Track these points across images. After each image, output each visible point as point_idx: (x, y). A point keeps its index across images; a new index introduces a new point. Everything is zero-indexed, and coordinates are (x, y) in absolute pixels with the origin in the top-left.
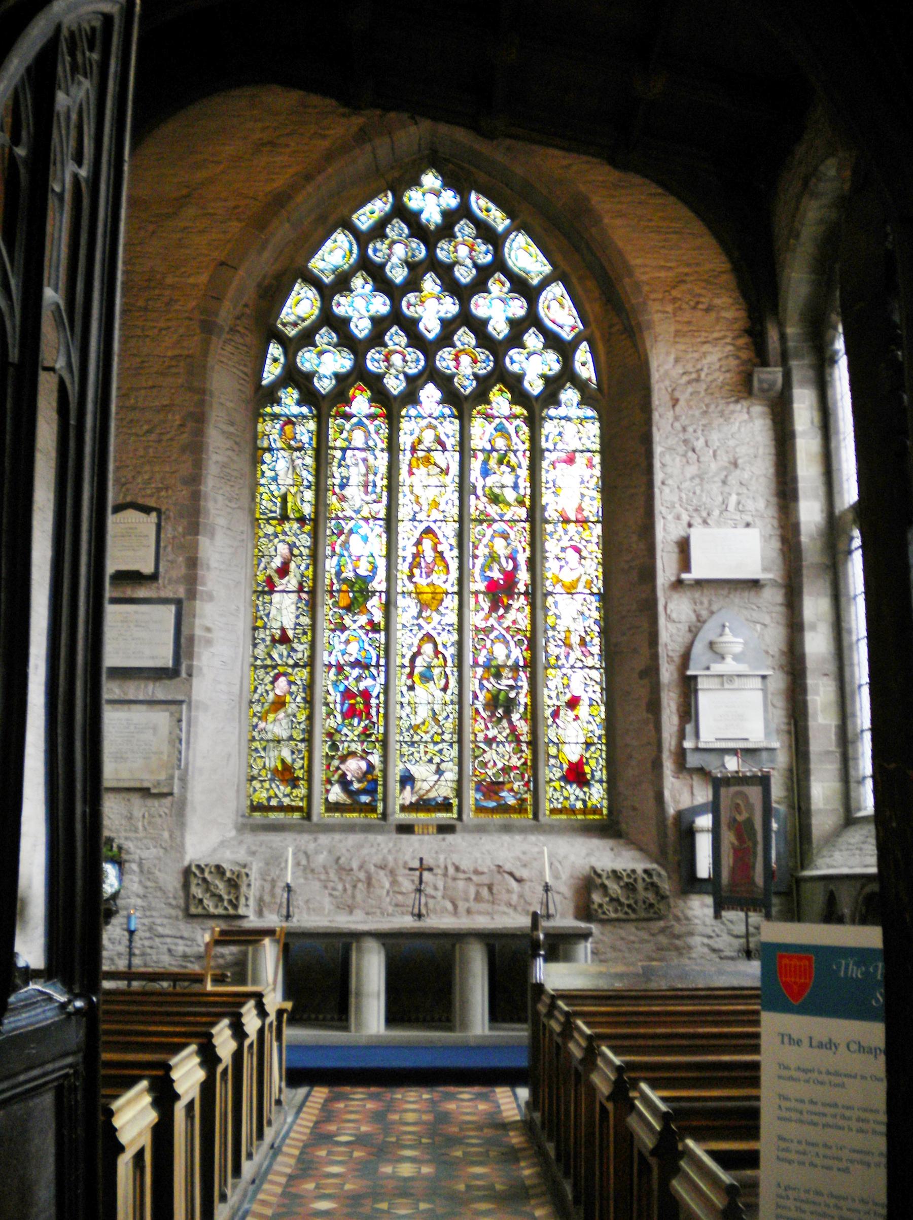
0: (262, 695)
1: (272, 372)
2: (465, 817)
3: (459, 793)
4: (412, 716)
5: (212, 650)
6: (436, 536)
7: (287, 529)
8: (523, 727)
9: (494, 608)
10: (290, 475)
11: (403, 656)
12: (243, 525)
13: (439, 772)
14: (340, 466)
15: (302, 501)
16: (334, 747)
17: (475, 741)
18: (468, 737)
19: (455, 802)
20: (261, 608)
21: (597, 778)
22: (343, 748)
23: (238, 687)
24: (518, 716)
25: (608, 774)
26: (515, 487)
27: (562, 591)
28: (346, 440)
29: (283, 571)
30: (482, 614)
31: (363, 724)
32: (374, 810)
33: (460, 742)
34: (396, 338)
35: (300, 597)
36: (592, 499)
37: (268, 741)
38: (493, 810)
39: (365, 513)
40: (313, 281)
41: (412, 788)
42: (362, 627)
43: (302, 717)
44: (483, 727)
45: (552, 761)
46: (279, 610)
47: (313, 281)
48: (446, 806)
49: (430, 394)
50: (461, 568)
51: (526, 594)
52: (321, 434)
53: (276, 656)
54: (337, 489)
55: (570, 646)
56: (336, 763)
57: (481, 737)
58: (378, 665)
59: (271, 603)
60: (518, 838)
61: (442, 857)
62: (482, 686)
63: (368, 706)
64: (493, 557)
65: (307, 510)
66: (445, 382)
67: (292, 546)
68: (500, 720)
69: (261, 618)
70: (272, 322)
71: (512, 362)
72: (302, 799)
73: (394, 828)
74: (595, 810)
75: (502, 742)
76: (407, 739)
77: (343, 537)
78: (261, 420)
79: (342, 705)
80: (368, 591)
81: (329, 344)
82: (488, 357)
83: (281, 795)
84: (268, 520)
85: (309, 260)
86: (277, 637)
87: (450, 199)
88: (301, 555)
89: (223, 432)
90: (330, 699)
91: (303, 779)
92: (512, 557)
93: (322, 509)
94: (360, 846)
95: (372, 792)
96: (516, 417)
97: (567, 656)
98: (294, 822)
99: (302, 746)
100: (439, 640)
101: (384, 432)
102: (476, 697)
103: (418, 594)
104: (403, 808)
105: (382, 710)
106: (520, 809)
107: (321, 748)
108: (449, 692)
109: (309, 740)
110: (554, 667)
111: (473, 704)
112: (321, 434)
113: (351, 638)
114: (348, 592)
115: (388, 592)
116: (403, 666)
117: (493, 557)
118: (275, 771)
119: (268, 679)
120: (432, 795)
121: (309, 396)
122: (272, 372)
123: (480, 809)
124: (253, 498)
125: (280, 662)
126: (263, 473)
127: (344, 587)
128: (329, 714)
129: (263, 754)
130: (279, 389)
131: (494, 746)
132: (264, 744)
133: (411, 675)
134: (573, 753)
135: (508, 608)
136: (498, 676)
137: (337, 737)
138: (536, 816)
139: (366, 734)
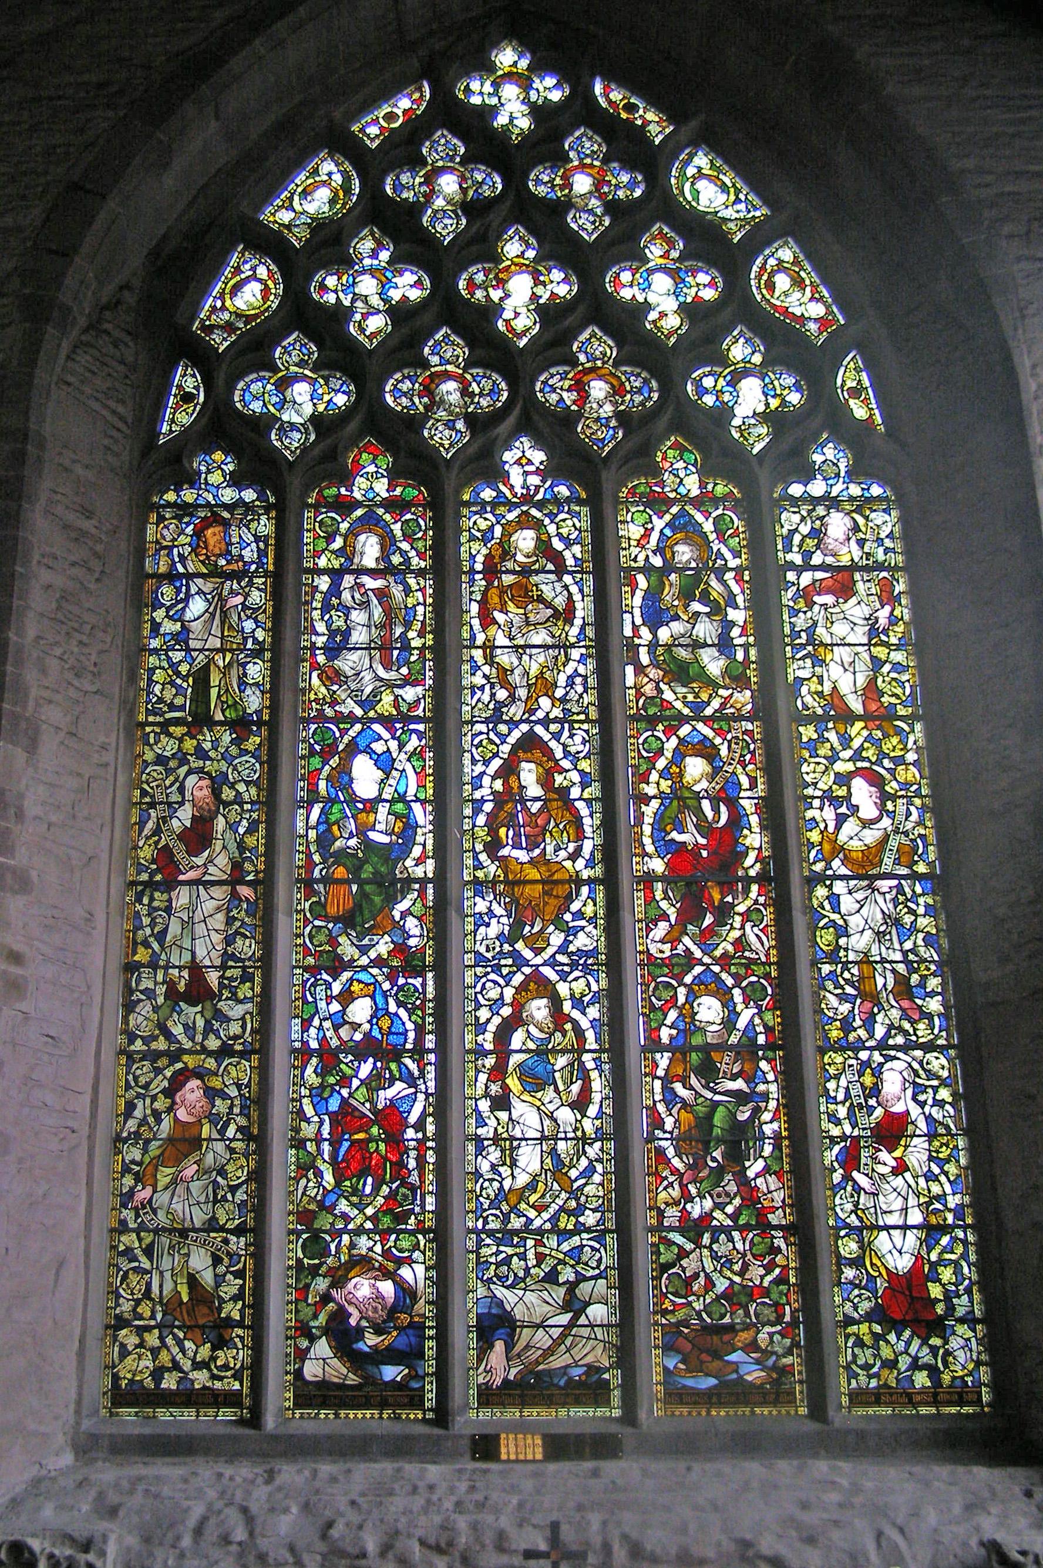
0: (143, 1122)
1: (177, 419)
2: (642, 1415)
3: (625, 1353)
4: (505, 1171)
5: (23, 1006)
6: (549, 753)
7: (207, 745)
8: (774, 1191)
9: (690, 913)
10: (216, 630)
11: (480, 1028)
12: (104, 726)
13: (575, 1305)
14: (326, 608)
15: (242, 684)
16: (316, 1245)
17: (660, 1228)
18: (643, 1219)
19: (614, 1377)
20: (146, 921)
21: (960, 1312)
22: (339, 1248)
23: (87, 1098)
24: (760, 1165)
25: (986, 1301)
26: (724, 645)
27: (844, 871)
28: (337, 553)
29: (199, 836)
30: (661, 929)
31: (385, 1190)
32: (416, 1401)
33: (624, 1231)
34: (445, 350)
35: (234, 894)
36: (897, 667)
37: (156, 1231)
38: (708, 1398)
39: (386, 704)
40: (270, 244)
41: (509, 1347)
42: (379, 962)
43: (238, 1173)
44: (676, 1193)
45: (849, 1273)
46: (188, 924)
47: (270, 244)
48: (590, 1388)
49: (523, 461)
50: (609, 826)
51: (762, 879)
52: (285, 542)
53: (177, 1030)
54: (321, 659)
55: (873, 998)
56: (321, 1284)
57: (672, 1215)
58: (419, 1051)
59: (168, 910)
60: (784, 1466)
61: (595, 1519)
62: (670, 1098)
63: (395, 1140)
64: (681, 799)
65: (254, 701)
66: (557, 430)
67: (217, 783)
68: (719, 1173)
69: (146, 944)
70: (180, 319)
71: (664, 458)
72: (237, 1376)
73: (465, 1443)
74: (961, 1394)
75: (726, 1230)
76: (493, 1225)
77: (334, 762)
78: (153, 517)
79: (335, 1144)
80: (394, 881)
81: (301, 364)
82: (646, 381)
83: (187, 1365)
84: (165, 725)
85: (259, 208)
86: (181, 987)
87: (550, 89)
88: (239, 800)
89: (66, 527)
90: (308, 1130)
91: (240, 1324)
92: (727, 796)
93: (286, 697)
94: (383, 1491)
95: (409, 1356)
96: (716, 501)
97: (869, 1023)
98: (221, 1430)
99: (237, 1244)
100: (563, 989)
101: (426, 537)
102: (657, 1123)
103: (510, 884)
104: (488, 1396)
105: (431, 1157)
106: (776, 1391)
107: (284, 1252)
108: (592, 1110)
109: (256, 1230)
110: (840, 1047)
111: (651, 1139)
112: (285, 542)
113: (356, 987)
114: (348, 882)
115: (440, 879)
116: (480, 1052)
117: (681, 799)
118: (171, 1305)
119: (160, 1083)
120: (557, 1362)
121: (259, 464)
122: (177, 419)
123: (676, 1395)
124: (133, 677)
125: (188, 1045)
126: (156, 627)
127: (340, 872)
128: (307, 1167)
129: (146, 1264)
130: (193, 455)
131: (706, 1239)
132: (148, 1238)
133: (498, 1073)
134: (897, 1252)
135: (724, 913)
136: (708, 1072)
137: (324, 1221)
138: (818, 1409)
139: (396, 1213)
